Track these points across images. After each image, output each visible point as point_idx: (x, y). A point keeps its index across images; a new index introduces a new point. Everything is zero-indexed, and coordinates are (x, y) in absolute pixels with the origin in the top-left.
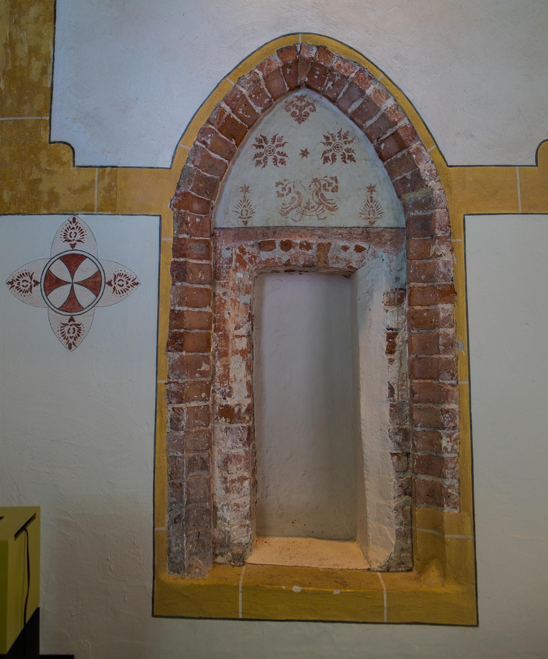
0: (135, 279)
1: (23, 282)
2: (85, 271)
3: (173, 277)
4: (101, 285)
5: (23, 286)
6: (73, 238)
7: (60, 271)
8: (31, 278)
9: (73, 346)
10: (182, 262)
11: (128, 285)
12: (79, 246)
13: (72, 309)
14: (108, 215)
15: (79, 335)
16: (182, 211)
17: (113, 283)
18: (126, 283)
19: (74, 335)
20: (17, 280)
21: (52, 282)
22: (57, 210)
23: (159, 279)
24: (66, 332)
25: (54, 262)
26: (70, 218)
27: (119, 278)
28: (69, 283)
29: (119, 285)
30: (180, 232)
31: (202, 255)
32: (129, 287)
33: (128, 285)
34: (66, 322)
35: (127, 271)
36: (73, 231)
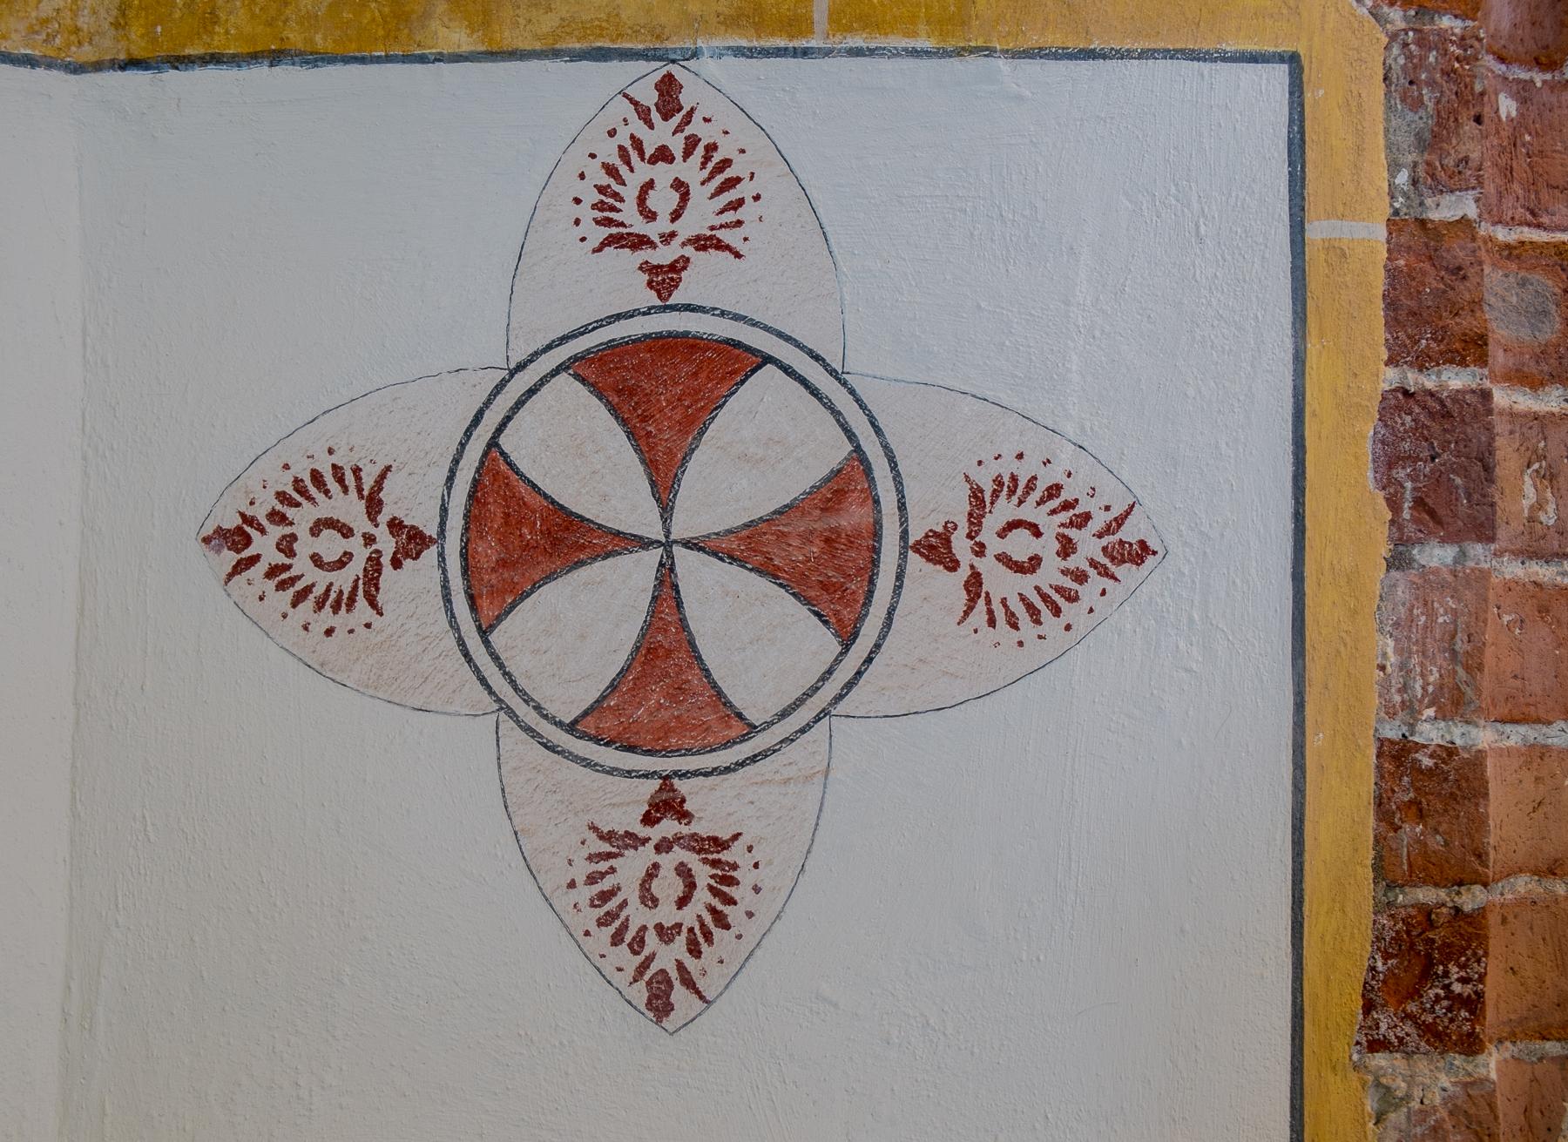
0: (1120, 521)
1: (315, 530)
2: (757, 454)
3: (1394, 504)
4: (875, 563)
5: (316, 560)
6: (663, 225)
7: (577, 453)
8: (374, 505)
9: (679, 994)
10: (1457, 396)
11: (1075, 562)
12: (705, 279)
13: (667, 731)
14: (915, 53)
15: (721, 921)
16: (1446, 22)
17: (961, 546)
18: (1057, 549)
19: (688, 916)
20: (277, 518)
21: (520, 537)
22: (548, 23)
23: (1299, 518)
24: (631, 893)
25: (532, 392)
26: (643, 80)
27: (1004, 511)
28: (645, 544)
29: (1004, 559)
30: (1438, 175)
31: (1542, 355)
32: (1081, 577)
33: (1077, 561)
34: (628, 819)
35: (1065, 457)
36: (663, 174)
